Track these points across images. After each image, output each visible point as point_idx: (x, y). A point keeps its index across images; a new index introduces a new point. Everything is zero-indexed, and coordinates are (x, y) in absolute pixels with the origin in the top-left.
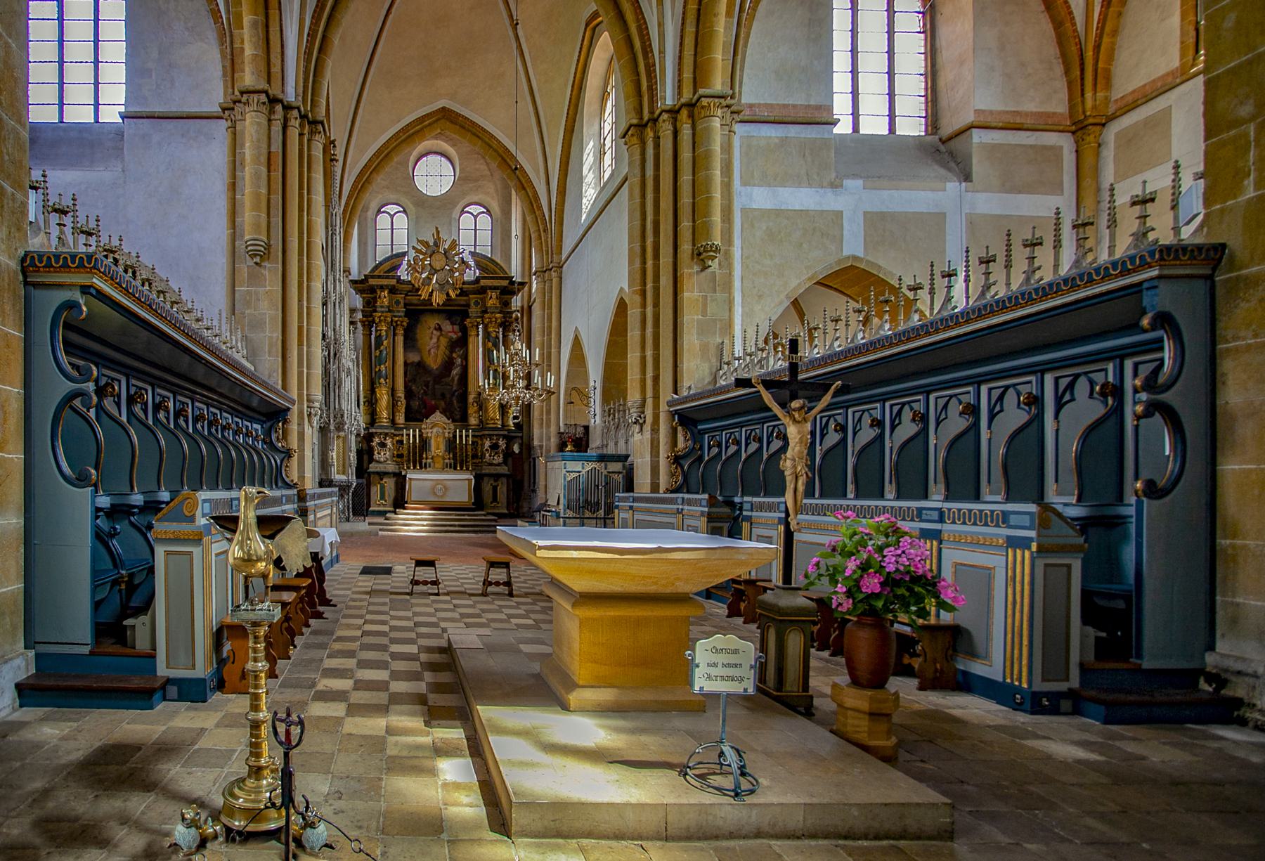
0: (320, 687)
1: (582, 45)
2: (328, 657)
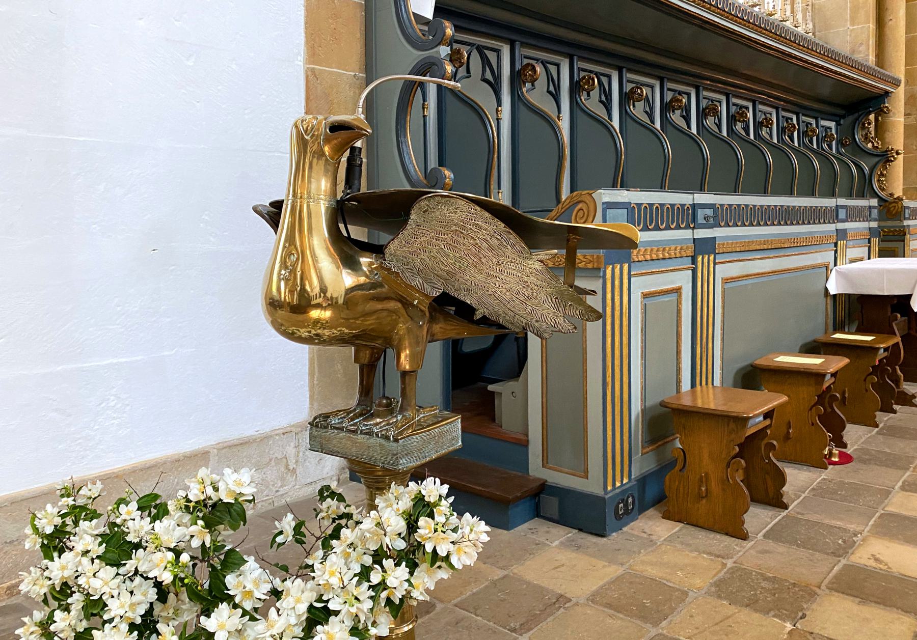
0: (862, 557)
2: (903, 488)
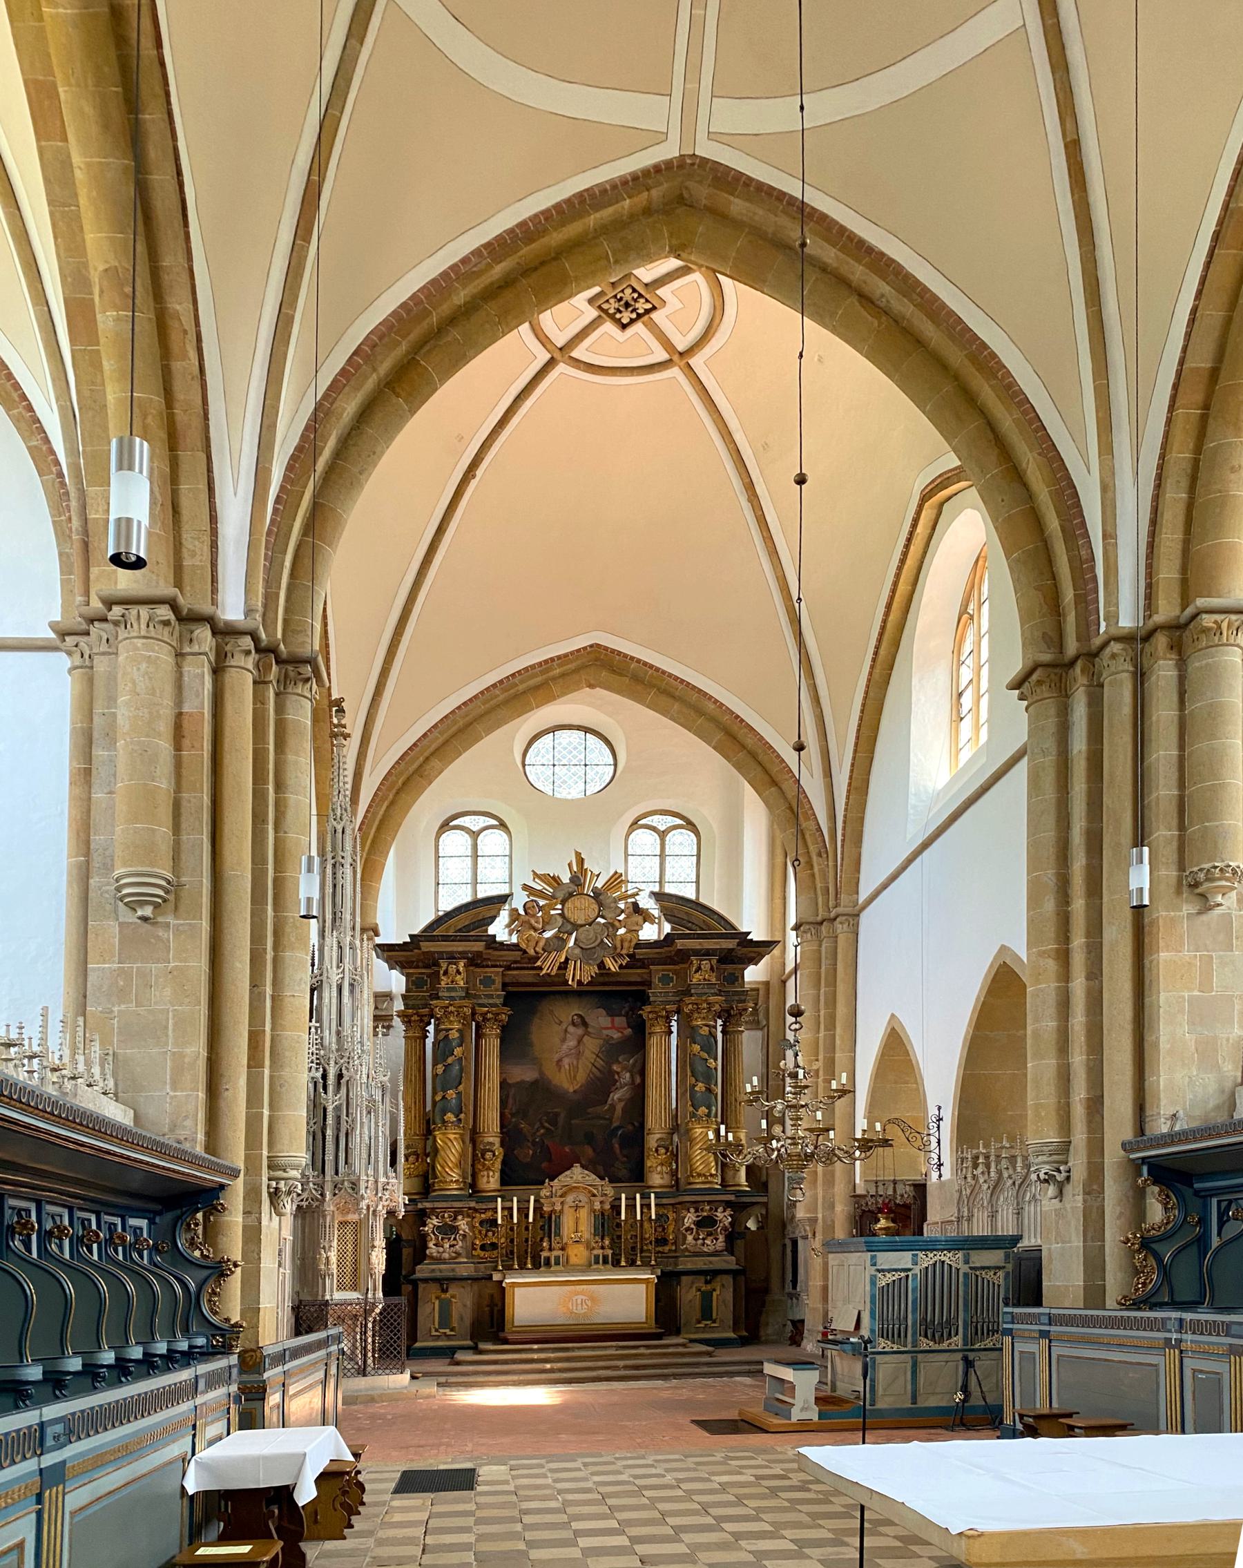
1: (911, 533)
